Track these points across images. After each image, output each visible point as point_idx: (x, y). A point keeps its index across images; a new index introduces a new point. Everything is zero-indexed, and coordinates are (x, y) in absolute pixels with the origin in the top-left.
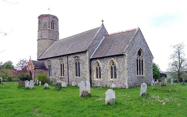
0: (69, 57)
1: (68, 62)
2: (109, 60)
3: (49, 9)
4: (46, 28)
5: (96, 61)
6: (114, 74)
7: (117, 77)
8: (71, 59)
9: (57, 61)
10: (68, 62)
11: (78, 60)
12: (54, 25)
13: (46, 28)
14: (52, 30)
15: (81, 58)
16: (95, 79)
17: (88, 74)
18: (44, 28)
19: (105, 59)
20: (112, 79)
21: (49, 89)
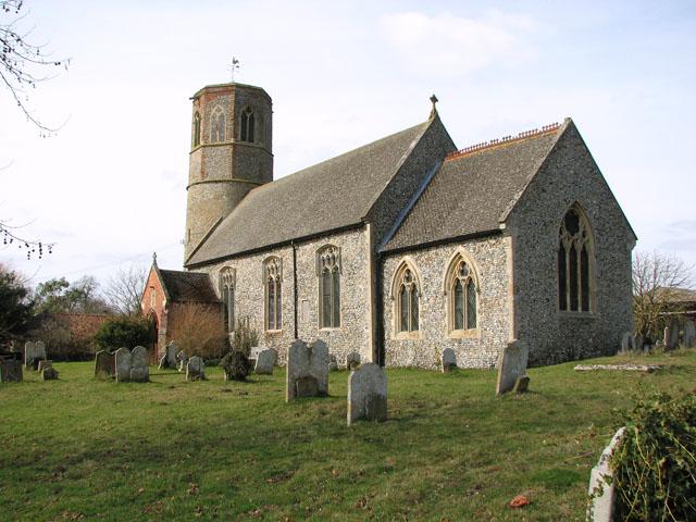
1: (295, 269)
2: (446, 255)
4: (222, 139)
5: (401, 261)
8: (308, 252)
10: (295, 269)
11: (332, 261)
12: (252, 125)
13: (222, 139)
18: (214, 138)
19: (433, 252)
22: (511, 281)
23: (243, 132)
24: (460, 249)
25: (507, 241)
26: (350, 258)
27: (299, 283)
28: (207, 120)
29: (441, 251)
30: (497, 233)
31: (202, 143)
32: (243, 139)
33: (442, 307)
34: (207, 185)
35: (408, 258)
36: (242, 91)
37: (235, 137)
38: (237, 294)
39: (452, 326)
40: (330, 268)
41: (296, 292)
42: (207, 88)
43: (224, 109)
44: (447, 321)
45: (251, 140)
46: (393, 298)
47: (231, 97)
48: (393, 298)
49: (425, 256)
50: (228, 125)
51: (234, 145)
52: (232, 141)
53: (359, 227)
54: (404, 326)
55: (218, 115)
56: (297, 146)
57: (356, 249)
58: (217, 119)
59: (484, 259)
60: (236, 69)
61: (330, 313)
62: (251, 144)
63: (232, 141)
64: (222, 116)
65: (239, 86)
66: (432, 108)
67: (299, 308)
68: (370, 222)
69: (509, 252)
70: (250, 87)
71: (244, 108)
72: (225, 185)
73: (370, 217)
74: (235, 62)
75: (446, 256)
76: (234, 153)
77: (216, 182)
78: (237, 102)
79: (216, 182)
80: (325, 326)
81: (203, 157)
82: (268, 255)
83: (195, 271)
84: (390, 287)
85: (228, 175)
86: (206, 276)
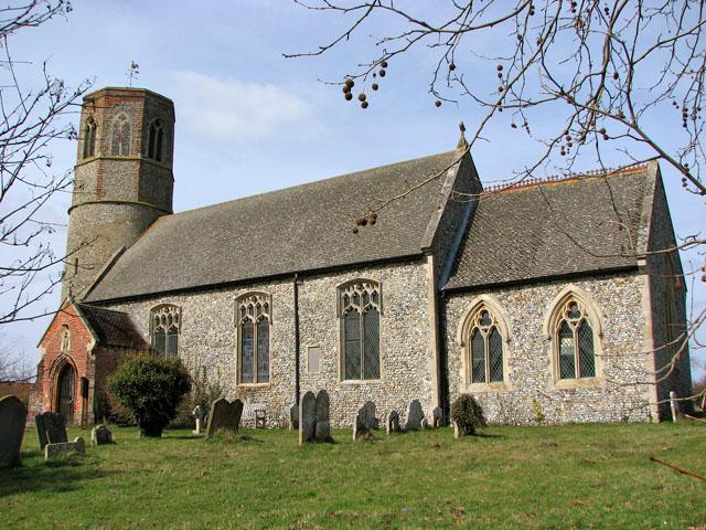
0: (307, 285)
1: (297, 308)
2: (552, 296)
3: (134, 67)
4: (125, 152)
5: (475, 301)
6: (578, 363)
7: (506, 375)
8: (321, 291)
9: (225, 302)
10: (297, 308)
11: (255, 310)
12: (160, 141)
13: (125, 152)
14: (153, 161)
15: (387, 290)
16: (462, 384)
17: (432, 365)
18: (115, 150)
19: (526, 292)
20: (568, 383)
21: (323, 447)
22: (648, 323)
23: (151, 148)
24: (571, 287)
25: (642, 282)
26: (397, 295)
27: (302, 326)
28: (105, 129)
29: (541, 290)
30: (632, 270)
31: (98, 154)
32: (151, 156)
33: (545, 354)
34: (105, 206)
35: (485, 297)
36: (153, 100)
37: (143, 152)
38: (182, 339)
39: (558, 375)
40: (254, 319)
41: (298, 336)
42: (108, 89)
43: (131, 118)
44: (552, 369)
45: (159, 159)
46: (463, 345)
47: (139, 105)
48: (463, 345)
49: (513, 295)
50: (135, 137)
51: (142, 162)
52: (139, 156)
53: (417, 259)
54: (476, 375)
55: (122, 123)
56: (197, 184)
57: (410, 287)
58: (120, 129)
59: (608, 300)
60: (135, 75)
61: (361, 358)
62: (158, 163)
63: (139, 156)
64: (127, 126)
65: (148, 93)
66: (460, 137)
67: (304, 355)
68: (434, 254)
69: (645, 292)
70: (160, 97)
71: (153, 120)
72: (129, 208)
73: (432, 250)
74: (134, 67)
75: (549, 296)
76: (142, 171)
77: (118, 203)
78: (146, 111)
79: (118, 203)
80: (348, 377)
81: (101, 171)
82: (244, 291)
83: (111, 309)
84: (458, 333)
85: (133, 196)
86: (124, 316)
